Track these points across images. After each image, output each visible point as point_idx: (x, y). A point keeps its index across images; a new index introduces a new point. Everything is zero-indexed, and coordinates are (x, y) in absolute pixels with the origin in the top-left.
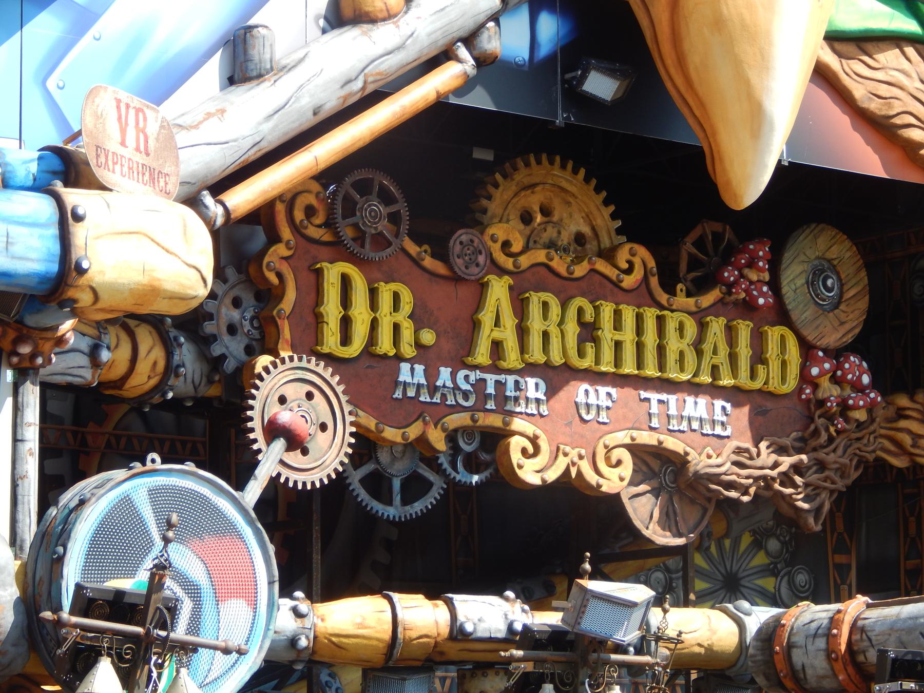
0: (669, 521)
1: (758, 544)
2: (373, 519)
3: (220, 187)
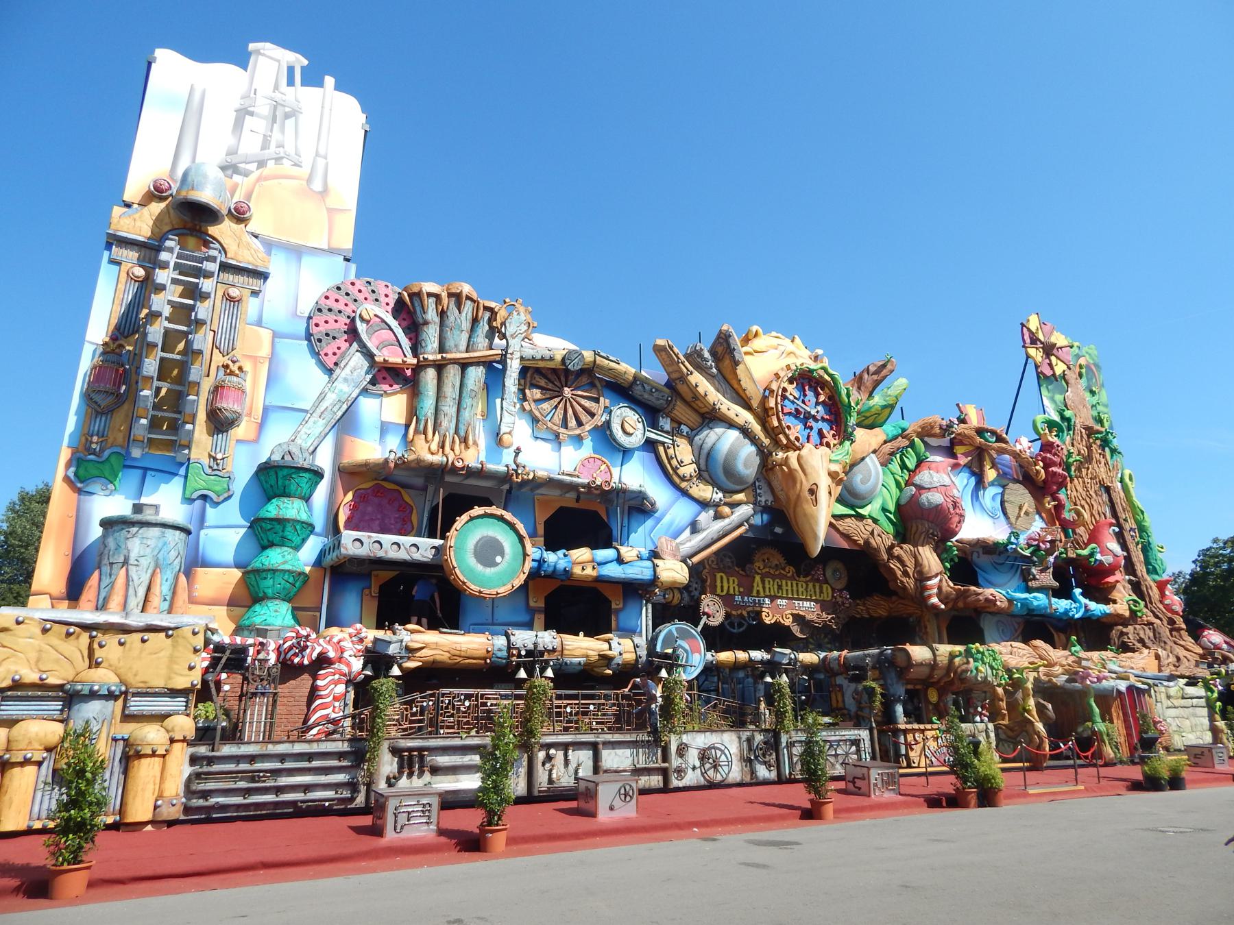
0: (801, 632)
1: (825, 637)
2: (732, 633)
3: (691, 557)
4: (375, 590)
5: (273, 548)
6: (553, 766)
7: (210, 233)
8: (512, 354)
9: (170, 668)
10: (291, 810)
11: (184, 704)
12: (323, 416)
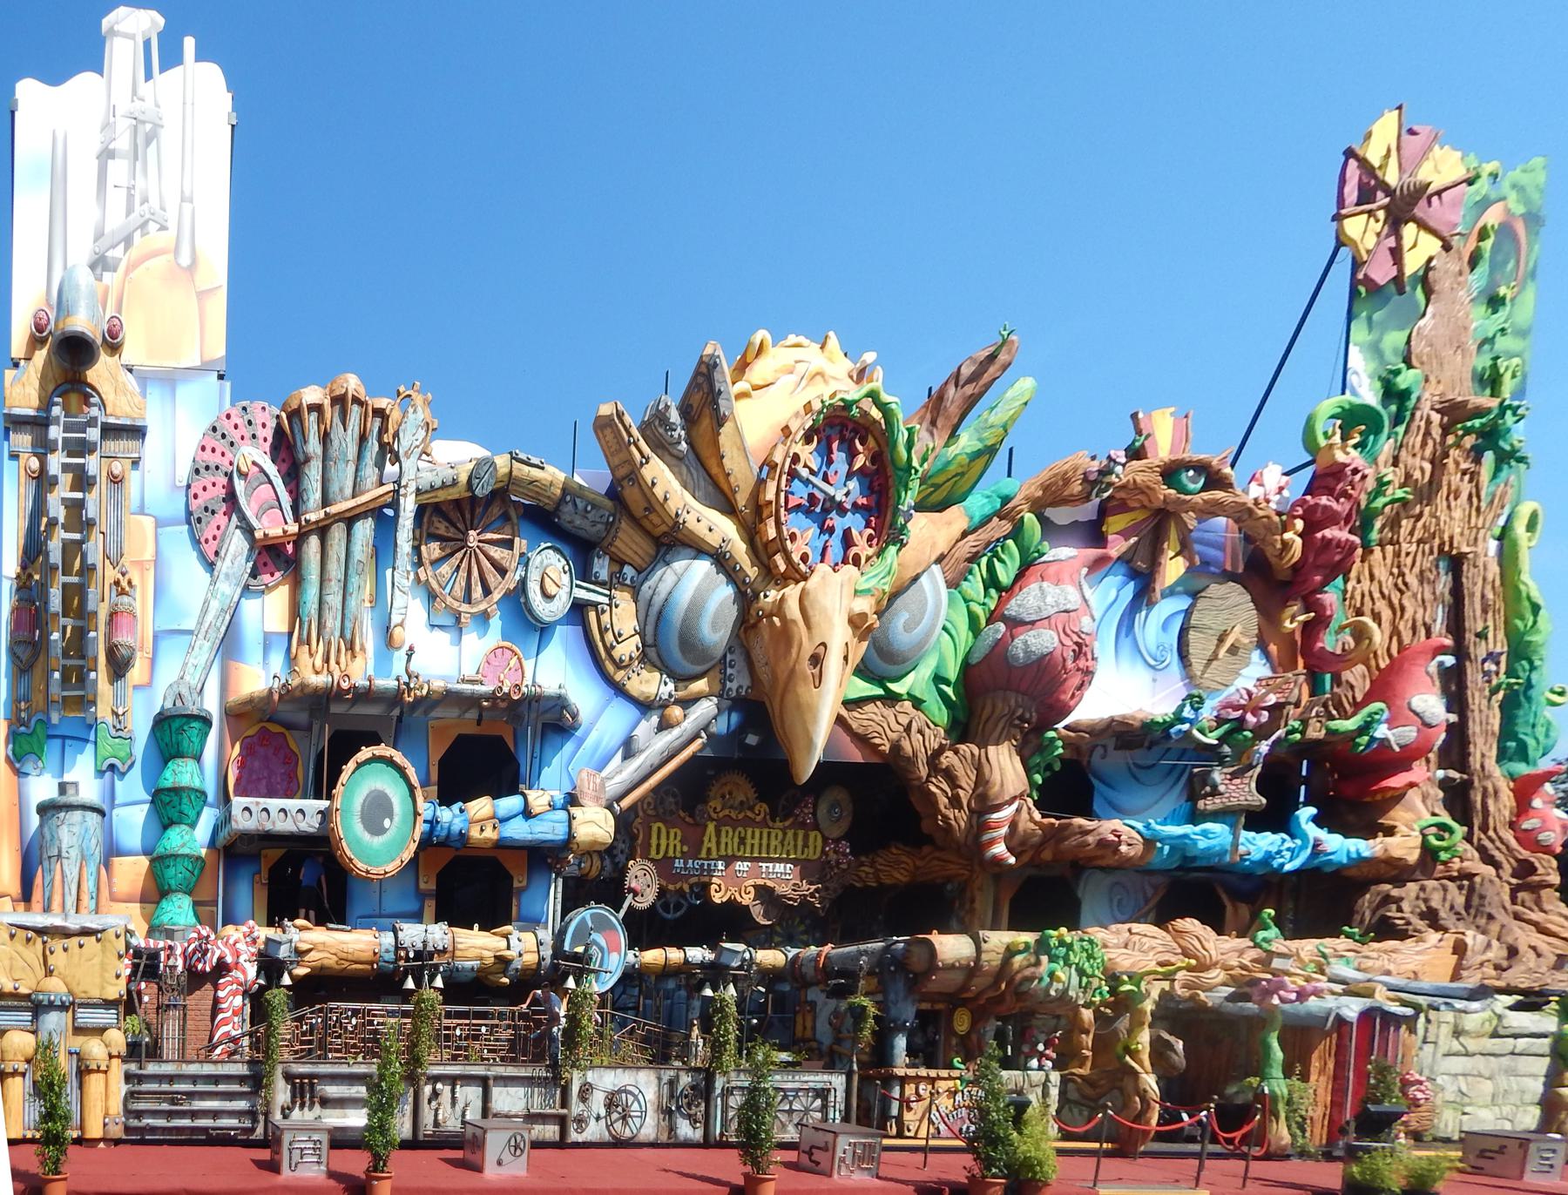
0: (766, 916)
1: (802, 922)
2: (664, 920)
4: (265, 874)
6: (439, 1104)
9: (102, 976)
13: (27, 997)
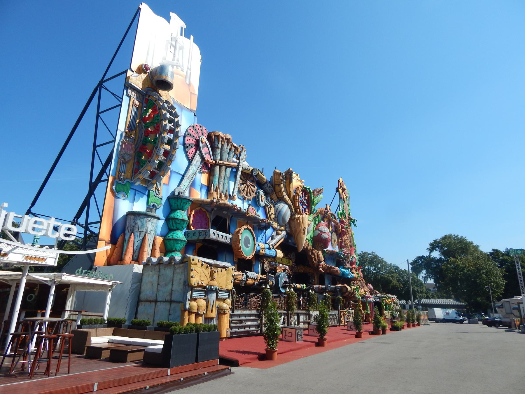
4: (196, 250)
5: (178, 231)
7: (159, 92)
8: (240, 166)
9: (226, 282)
10: (247, 334)
11: (228, 295)
12: (189, 178)
13: (205, 287)
